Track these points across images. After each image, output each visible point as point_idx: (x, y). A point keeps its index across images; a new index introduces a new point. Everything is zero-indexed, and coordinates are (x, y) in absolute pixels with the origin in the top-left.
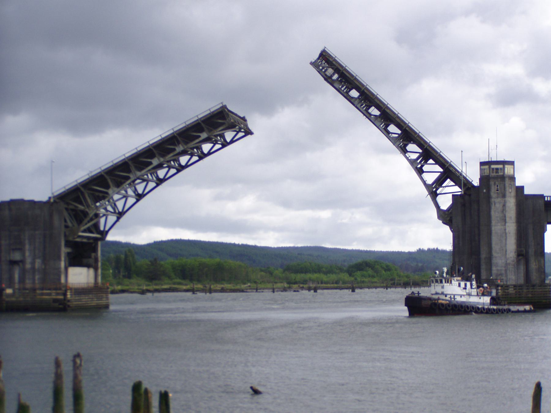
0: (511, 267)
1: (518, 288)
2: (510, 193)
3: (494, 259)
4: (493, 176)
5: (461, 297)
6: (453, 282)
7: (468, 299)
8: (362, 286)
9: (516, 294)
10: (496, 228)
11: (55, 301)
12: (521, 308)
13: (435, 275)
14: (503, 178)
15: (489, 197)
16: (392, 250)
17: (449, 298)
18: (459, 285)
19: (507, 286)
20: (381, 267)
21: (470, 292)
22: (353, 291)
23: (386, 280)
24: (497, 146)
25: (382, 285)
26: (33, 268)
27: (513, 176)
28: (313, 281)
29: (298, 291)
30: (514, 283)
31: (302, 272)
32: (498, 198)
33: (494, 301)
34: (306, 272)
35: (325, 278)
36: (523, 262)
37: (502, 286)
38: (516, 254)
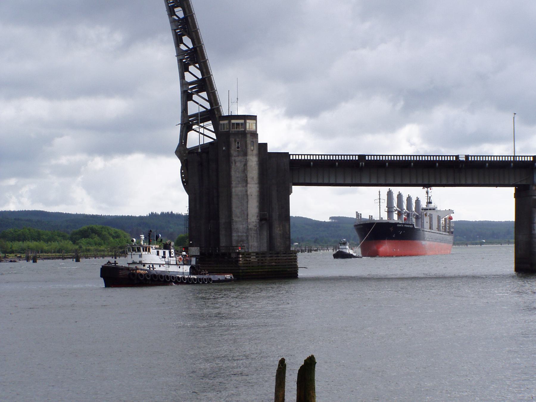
0: (252, 233)
1: (261, 255)
3: (234, 224)
4: (233, 132)
5: (160, 266)
7: (167, 269)
8: (87, 255)
9: (258, 263)
10: (237, 190)
12: (221, 277)
13: (132, 242)
14: (244, 134)
15: (228, 156)
16: (121, 215)
17: (148, 267)
18: (158, 254)
19: (249, 254)
20: (109, 233)
21: (169, 261)
22: (78, 261)
23: (114, 248)
24: (237, 98)
25: (110, 253)
27: (255, 132)
28: (32, 250)
29: (15, 261)
31: (19, 240)
32: (238, 156)
33: (193, 270)
34: (23, 240)
35: (45, 246)
37: (243, 254)
38: (259, 218)
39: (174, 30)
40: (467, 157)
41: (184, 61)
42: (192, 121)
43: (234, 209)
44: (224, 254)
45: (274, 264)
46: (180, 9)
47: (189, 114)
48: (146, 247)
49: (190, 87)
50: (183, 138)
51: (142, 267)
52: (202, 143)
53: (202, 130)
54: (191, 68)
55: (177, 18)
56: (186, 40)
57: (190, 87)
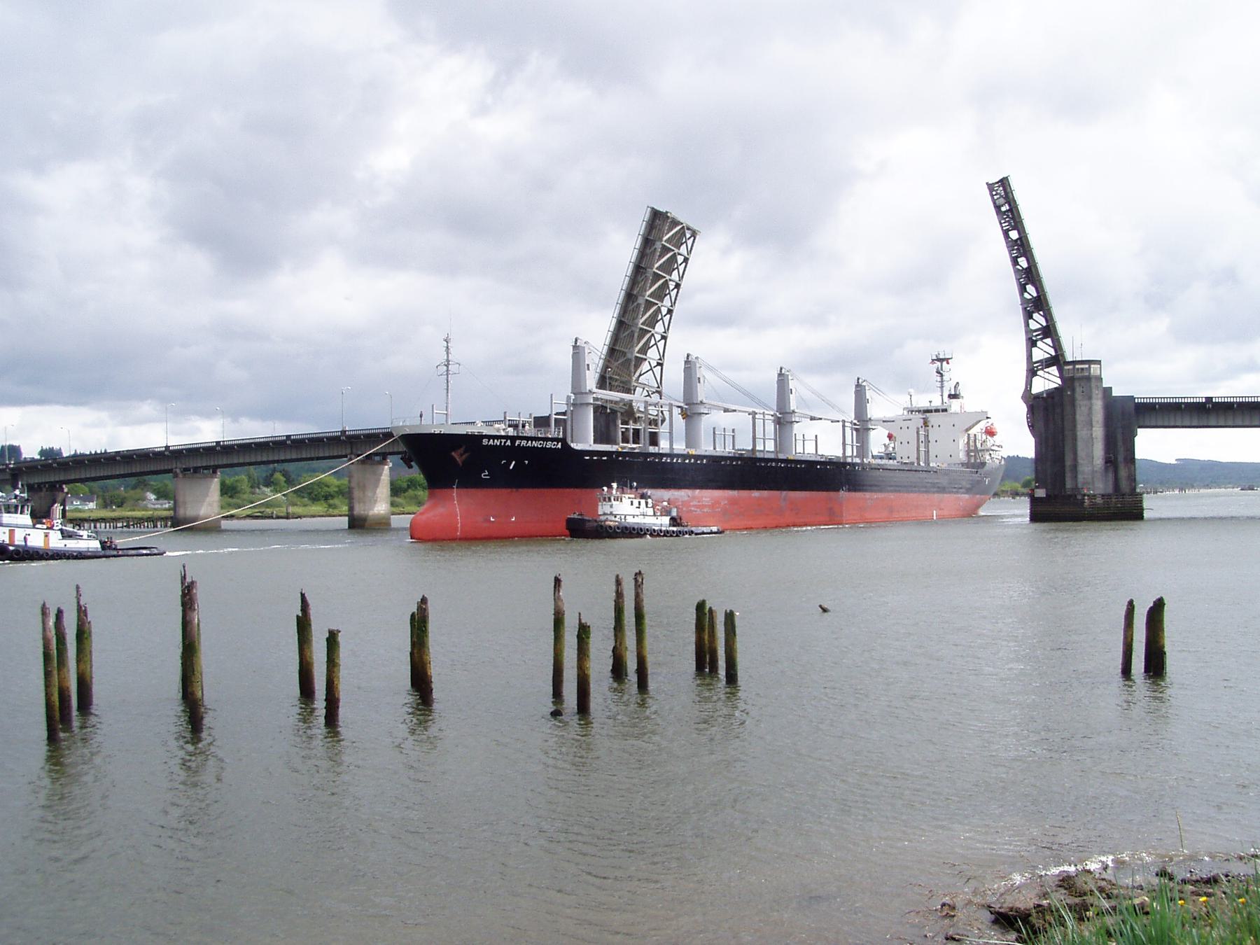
2: (1097, 394)
6: (623, 499)
10: (1082, 433)
14: (1088, 378)
18: (632, 504)
30: (1102, 492)
37: (1088, 496)
39: (1018, 280)
41: (1028, 309)
42: (1037, 367)
43: (1079, 449)
44: (1070, 496)
45: (1119, 505)
46: (1023, 259)
47: (1034, 360)
48: (618, 497)
49: (1034, 334)
50: (1029, 384)
51: (613, 518)
52: (1047, 388)
53: (1047, 376)
54: (1036, 316)
55: (1021, 268)
56: (1030, 288)
57: (1034, 334)
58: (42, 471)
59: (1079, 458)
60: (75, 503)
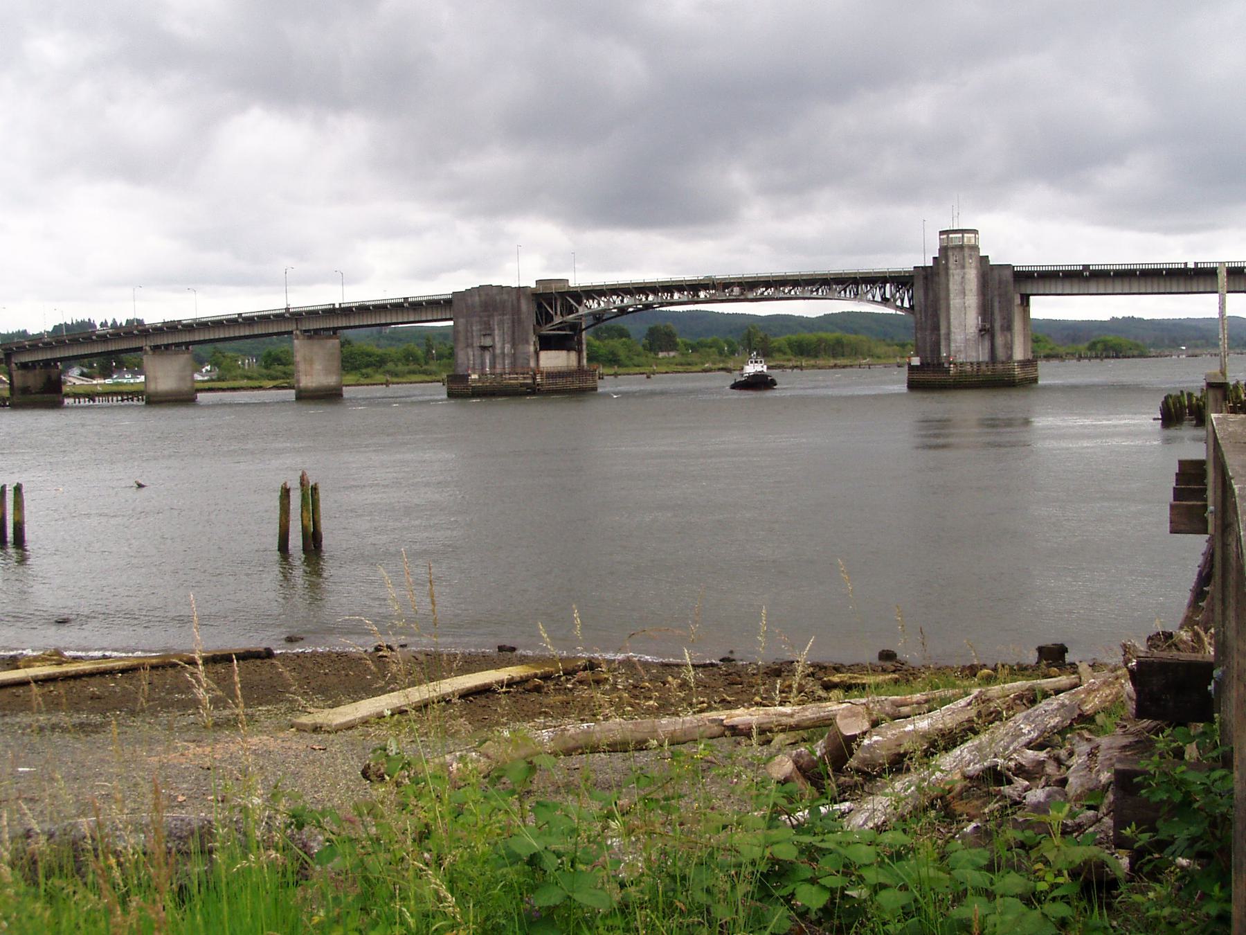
10: (955, 301)
11: (522, 385)
15: (947, 268)
26: (503, 353)
32: (956, 269)
36: (987, 337)
40: (1196, 264)
43: (952, 318)
58: (153, 334)
59: (952, 327)
60: (126, 376)
